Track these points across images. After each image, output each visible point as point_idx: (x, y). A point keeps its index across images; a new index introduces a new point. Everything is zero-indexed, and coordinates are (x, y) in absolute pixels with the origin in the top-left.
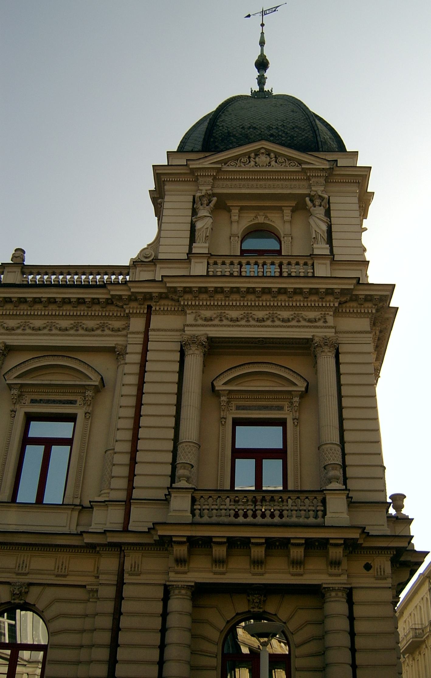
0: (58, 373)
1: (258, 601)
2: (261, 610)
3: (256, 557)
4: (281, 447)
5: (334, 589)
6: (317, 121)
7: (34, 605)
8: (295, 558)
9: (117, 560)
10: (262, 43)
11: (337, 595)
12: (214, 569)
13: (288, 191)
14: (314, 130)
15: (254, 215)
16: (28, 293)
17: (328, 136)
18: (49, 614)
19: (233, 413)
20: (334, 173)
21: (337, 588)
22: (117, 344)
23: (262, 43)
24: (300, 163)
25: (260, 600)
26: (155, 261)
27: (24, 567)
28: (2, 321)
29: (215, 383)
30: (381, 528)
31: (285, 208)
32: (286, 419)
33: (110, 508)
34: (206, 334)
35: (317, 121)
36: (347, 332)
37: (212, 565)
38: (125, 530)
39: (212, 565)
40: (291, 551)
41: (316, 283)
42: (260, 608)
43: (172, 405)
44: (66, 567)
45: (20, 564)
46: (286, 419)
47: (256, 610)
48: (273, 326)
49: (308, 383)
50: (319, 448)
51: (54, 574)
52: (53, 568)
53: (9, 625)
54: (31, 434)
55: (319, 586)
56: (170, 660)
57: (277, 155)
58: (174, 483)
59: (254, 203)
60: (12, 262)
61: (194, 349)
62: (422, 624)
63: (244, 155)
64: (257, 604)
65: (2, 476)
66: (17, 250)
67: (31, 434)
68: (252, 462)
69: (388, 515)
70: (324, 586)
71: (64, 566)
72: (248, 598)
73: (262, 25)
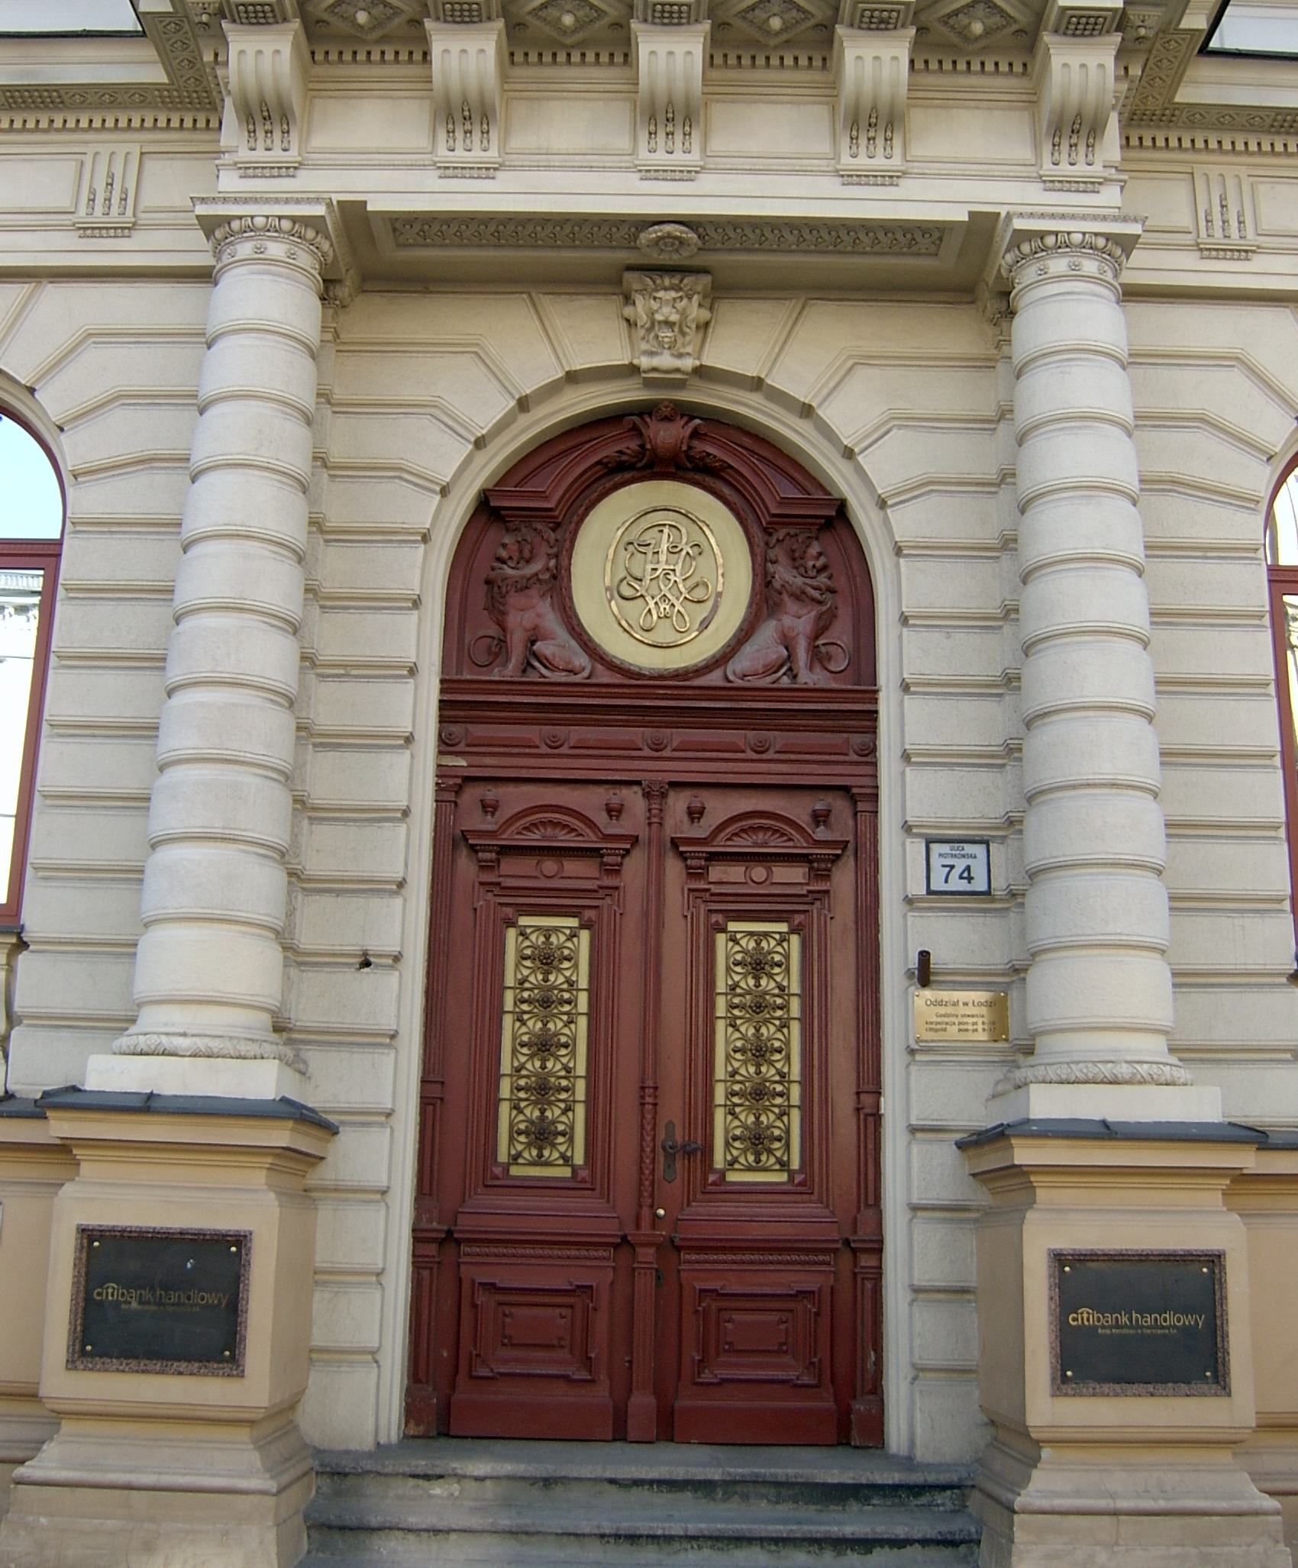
1: (675, 317)
2: (688, 364)
5: (1063, 244)
8: (1091, 97)
11: (1075, 267)
12: (644, 154)
18: (74, 449)
21: (1077, 238)
25: (683, 313)
27: (115, 200)
37: (635, 139)
39: (635, 139)
40: (1056, 62)
42: (680, 356)
44: (125, 192)
45: (93, 192)
47: (666, 361)
52: (66, 203)
55: (982, 228)
56: (1041, 567)
64: (666, 334)
70: (1019, 224)
71: (117, 186)
72: (628, 311)
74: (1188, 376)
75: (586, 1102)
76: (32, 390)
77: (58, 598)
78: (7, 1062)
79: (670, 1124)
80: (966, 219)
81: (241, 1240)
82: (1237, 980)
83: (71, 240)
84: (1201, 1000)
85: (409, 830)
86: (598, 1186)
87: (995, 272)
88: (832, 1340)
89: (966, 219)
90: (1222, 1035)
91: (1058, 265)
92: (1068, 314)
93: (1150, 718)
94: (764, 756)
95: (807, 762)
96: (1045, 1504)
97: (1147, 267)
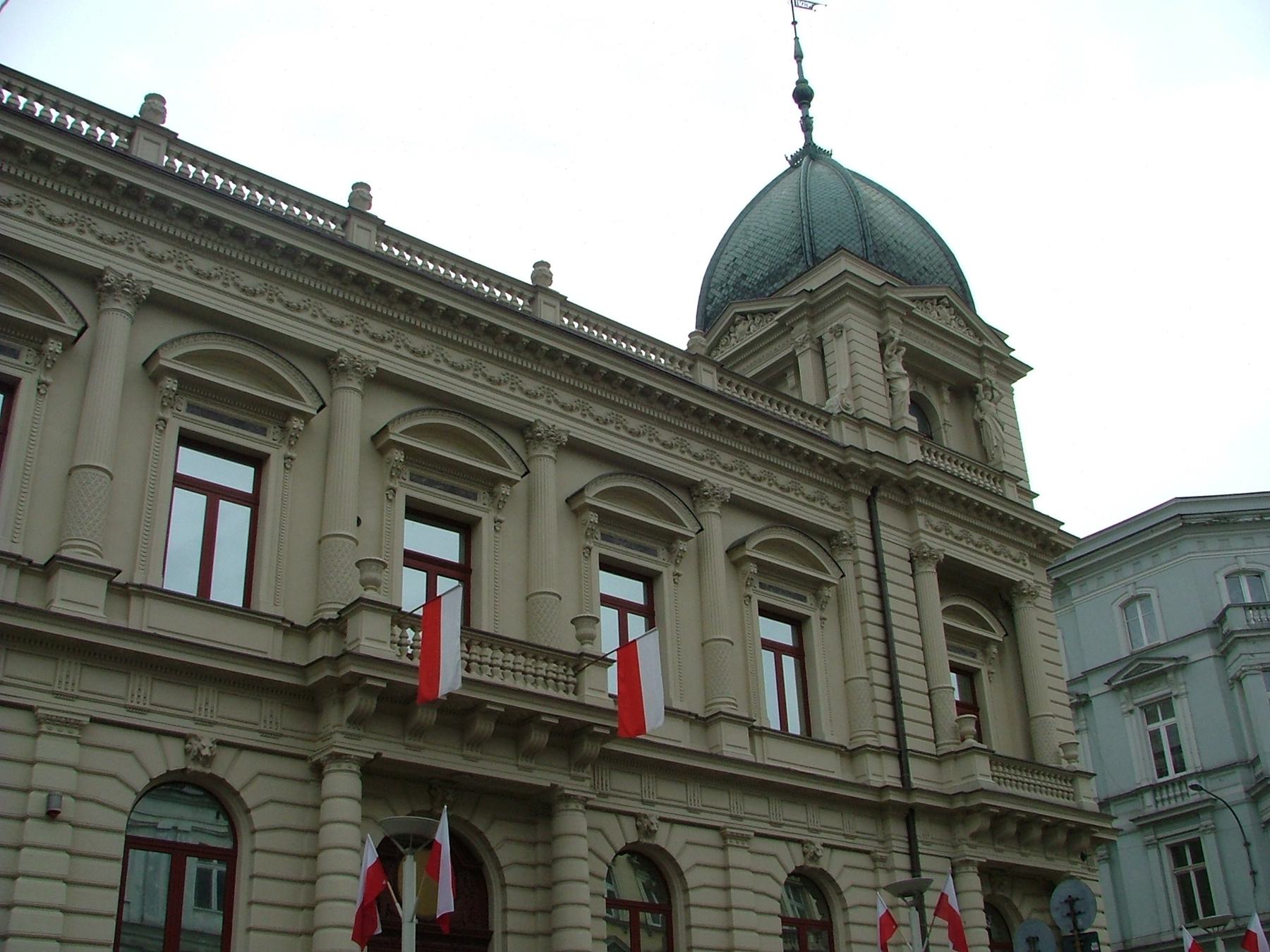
0: (1252, 735)
3: (871, 214)
4: (131, 851)
6: (856, 181)
7: (248, 811)
9: (723, 724)
10: (799, 57)
13: (773, 361)
14: (855, 195)
15: (762, 526)
16: (30, 134)
17: (893, 217)
19: (184, 419)
20: (885, 513)
22: (109, 267)
23: (799, 57)
24: (776, 312)
26: (719, 311)
28: (14, 774)
29: (161, 352)
30: (743, 752)
31: (744, 366)
32: (19, 380)
33: (1075, 592)
34: (151, 282)
35: (856, 181)
36: (331, 926)
38: (505, 933)
41: (22, 130)
43: (132, 788)
46: (19, 380)
48: (354, 339)
49: (260, 774)
50: (320, 542)
51: (259, 731)
53: (199, 870)
54: (224, 505)
57: (753, 314)
58: (368, 795)
59: (109, 700)
60: (530, 282)
61: (124, 302)
62: (932, 926)
63: (931, 298)
65: (3, 5)
66: (148, 97)
67: (224, 505)
68: (216, 595)
69: (805, 735)
73: (794, 23)
74: (279, 925)
75: (175, 843)
76: (254, 832)
77: (500, 682)
78: (796, 38)
79: (942, 403)
80: (652, 292)
81: (181, 428)
82: (236, 723)
83: (257, 736)
84: (871, 902)
85: (885, 525)
86: (148, 278)
87: (61, 314)
88: (103, 804)
89: (652, 292)
90: (88, 793)
91: (573, 806)
92: (574, 821)
93: (359, 826)
94: (462, 374)
95: (20, 687)
96: (106, 691)
97: (589, 803)
